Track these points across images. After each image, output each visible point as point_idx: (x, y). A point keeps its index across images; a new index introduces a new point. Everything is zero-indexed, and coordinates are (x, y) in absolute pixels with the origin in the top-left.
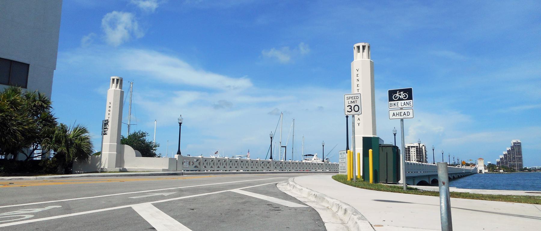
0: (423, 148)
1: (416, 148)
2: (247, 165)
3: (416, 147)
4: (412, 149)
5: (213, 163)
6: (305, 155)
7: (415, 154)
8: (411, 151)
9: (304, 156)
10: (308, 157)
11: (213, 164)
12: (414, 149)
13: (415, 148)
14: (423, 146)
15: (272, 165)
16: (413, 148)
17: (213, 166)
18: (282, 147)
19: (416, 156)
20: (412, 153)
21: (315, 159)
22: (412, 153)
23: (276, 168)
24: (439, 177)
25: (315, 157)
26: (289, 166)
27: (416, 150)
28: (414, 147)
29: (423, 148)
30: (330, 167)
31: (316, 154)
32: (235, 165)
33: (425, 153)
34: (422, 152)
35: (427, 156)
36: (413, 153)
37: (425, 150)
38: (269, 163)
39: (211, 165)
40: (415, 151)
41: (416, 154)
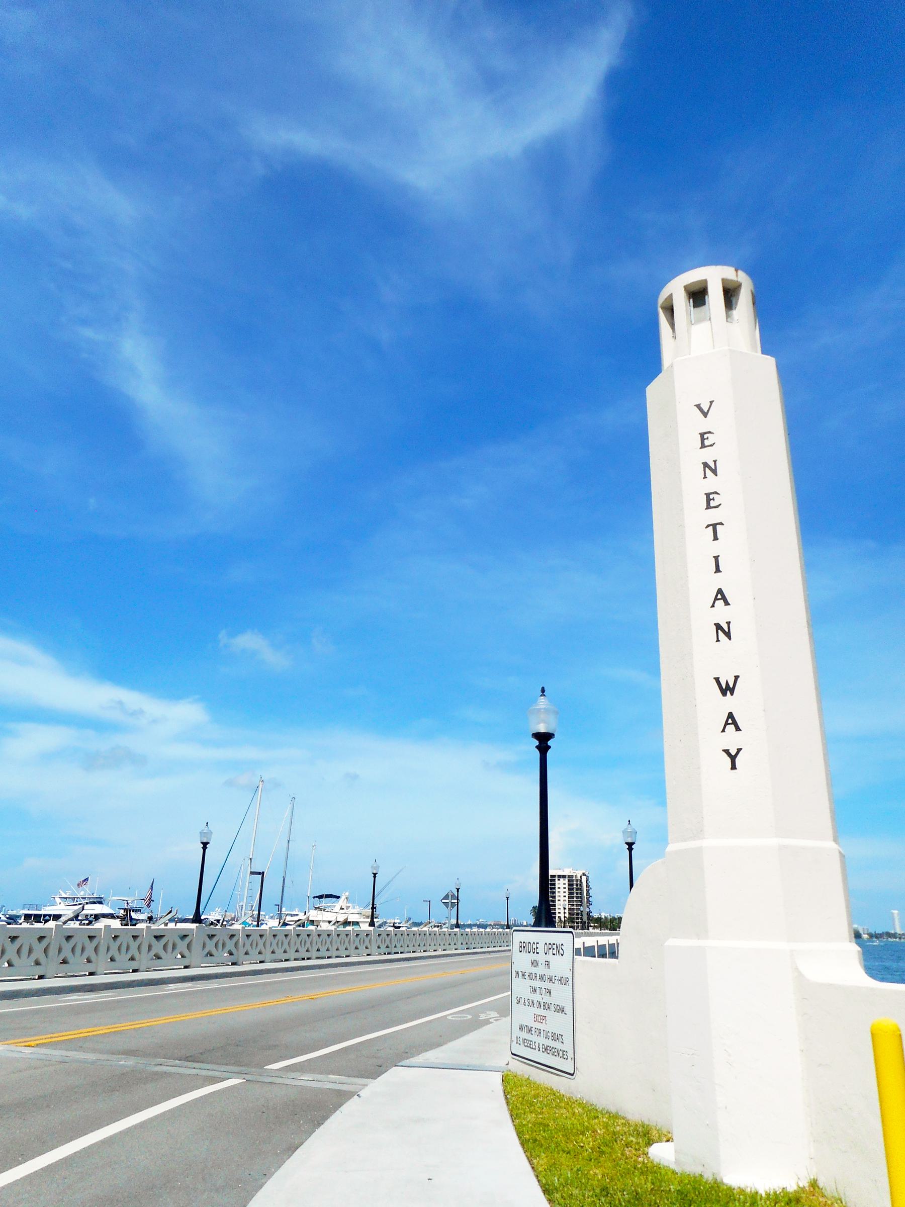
0: (584, 878)
1: (569, 881)
2: (134, 951)
3: (569, 876)
4: (559, 882)
5: (288, 941)
6: (317, 897)
7: (567, 894)
8: (557, 886)
9: (314, 897)
10: (325, 902)
11: (216, 947)
12: (564, 882)
13: (567, 879)
14: (584, 874)
15: (196, 947)
16: (562, 879)
17: (137, 955)
18: (252, 873)
19: (567, 898)
20: (559, 892)
21: (342, 909)
22: (559, 892)
23: (158, 957)
24: (862, 968)
25: (342, 902)
26: (261, 946)
27: (569, 885)
28: (564, 877)
29: (584, 878)
30: (390, 940)
31: (347, 894)
32: (128, 949)
33: (588, 891)
34: (581, 889)
35: (590, 899)
36: (562, 890)
37: (588, 886)
38: (187, 940)
39: (365, 943)
40: (566, 886)
41: (567, 893)
